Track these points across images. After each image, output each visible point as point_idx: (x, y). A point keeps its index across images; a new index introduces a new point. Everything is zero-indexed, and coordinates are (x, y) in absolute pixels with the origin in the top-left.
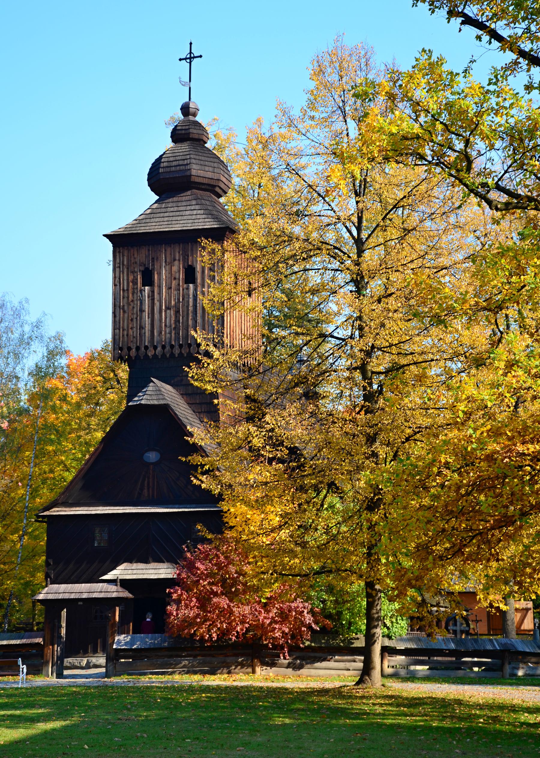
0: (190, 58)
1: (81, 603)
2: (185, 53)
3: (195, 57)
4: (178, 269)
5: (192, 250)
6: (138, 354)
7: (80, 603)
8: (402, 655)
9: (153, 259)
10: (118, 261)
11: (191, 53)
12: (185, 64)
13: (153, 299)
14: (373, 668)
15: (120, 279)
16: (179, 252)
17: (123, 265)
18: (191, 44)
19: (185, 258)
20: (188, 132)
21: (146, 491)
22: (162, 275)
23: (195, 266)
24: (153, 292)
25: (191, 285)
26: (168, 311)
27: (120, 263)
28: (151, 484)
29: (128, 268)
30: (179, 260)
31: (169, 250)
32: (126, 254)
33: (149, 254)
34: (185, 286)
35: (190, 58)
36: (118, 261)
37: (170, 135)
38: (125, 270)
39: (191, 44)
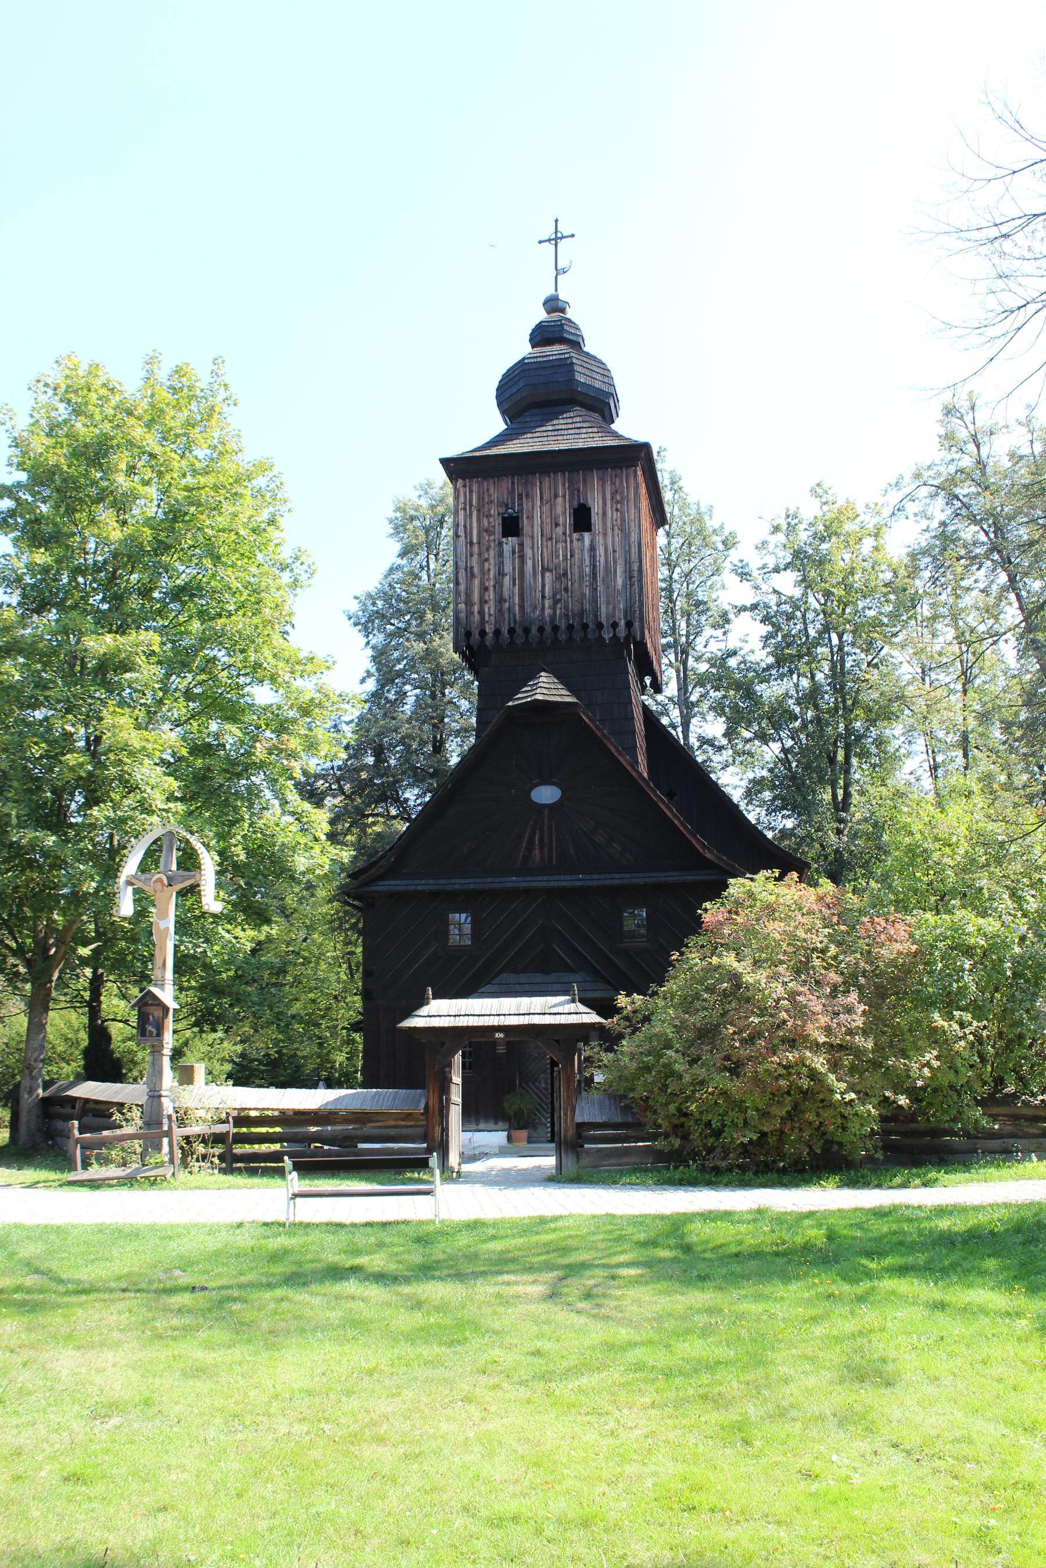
0: (556, 239)
1: (501, 1035)
2: (550, 233)
3: (563, 237)
4: (563, 509)
5: (585, 481)
7: (499, 1035)
9: (520, 496)
10: (462, 499)
11: (549, 240)
13: (522, 557)
14: (852, 1183)
17: (471, 505)
18: (556, 221)
19: (574, 491)
21: (537, 852)
24: (521, 545)
26: (548, 574)
28: (546, 841)
29: (479, 511)
30: (564, 497)
31: (546, 481)
32: (475, 488)
33: (513, 489)
34: (575, 536)
35: (556, 239)
36: (462, 499)
37: (496, 384)
39: (556, 221)
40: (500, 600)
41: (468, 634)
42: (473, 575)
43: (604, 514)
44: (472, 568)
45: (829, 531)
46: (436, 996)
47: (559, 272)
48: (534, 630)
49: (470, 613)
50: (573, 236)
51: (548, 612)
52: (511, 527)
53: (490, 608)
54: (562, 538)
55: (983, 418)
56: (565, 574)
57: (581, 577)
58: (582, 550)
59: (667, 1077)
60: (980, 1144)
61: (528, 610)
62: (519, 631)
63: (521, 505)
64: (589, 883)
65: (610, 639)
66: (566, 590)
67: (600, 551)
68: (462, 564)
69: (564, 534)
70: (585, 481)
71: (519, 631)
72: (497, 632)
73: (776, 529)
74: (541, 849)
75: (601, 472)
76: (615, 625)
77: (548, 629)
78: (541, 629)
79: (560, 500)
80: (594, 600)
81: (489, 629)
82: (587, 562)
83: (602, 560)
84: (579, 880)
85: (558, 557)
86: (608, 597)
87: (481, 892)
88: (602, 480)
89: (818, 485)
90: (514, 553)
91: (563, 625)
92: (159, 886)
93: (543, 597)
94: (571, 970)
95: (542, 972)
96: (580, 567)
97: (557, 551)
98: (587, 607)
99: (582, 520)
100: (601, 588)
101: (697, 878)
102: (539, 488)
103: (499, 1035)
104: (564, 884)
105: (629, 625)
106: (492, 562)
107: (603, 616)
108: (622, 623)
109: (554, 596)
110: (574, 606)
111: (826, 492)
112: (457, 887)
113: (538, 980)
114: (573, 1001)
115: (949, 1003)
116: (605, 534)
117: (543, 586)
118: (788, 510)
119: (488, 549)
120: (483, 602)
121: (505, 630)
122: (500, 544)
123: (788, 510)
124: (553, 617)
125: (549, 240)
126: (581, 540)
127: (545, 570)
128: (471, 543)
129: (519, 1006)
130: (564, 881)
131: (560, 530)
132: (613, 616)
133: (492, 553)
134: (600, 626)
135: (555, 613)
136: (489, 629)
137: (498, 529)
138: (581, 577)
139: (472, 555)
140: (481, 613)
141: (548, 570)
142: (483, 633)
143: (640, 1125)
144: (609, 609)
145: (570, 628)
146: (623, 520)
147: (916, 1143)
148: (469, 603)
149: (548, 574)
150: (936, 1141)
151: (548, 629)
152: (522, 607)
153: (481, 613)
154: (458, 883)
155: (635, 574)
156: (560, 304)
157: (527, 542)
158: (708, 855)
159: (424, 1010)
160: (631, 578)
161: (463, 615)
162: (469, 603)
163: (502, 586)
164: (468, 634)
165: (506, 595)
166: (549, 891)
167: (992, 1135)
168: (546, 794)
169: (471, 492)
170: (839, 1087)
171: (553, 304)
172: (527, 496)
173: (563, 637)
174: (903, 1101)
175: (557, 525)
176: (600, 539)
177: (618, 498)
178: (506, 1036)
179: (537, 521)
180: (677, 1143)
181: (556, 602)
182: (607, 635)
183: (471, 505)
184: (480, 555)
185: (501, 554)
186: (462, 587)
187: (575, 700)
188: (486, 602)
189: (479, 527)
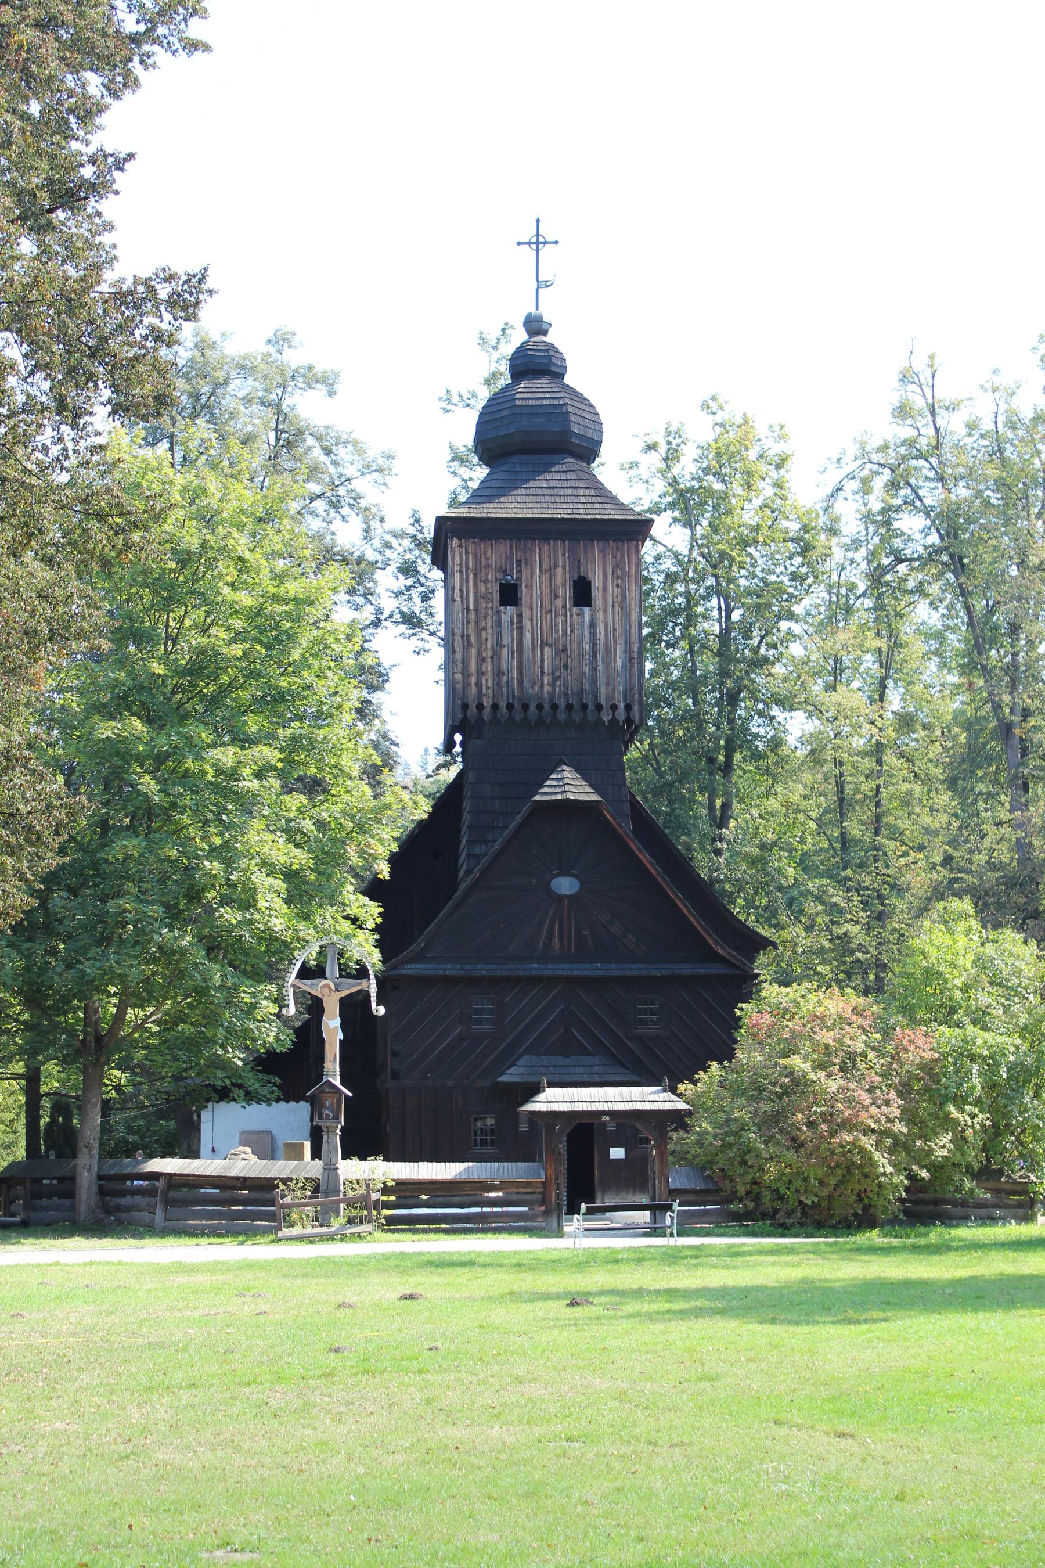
0: (538, 243)
2: (529, 234)
4: (563, 578)
5: (585, 552)
6: (525, 716)
7: (605, 1118)
8: (28, 1150)
9: (519, 562)
11: (529, 243)
12: (529, 252)
13: (520, 628)
15: (461, 590)
16: (564, 555)
17: (467, 568)
18: (538, 221)
19: (576, 564)
20: (536, 363)
22: (535, 589)
23: (590, 577)
24: (520, 616)
25: (586, 610)
26: (547, 649)
27: (461, 565)
29: (475, 575)
31: (546, 548)
34: (575, 610)
35: (538, 243)
38: (471, 577)
39: (538, 221)
40: (498, 673)
41: (465, 707)
42: (469, 644)
43: (605, 589)
44: (469, 636)
45: (723, 458)
46: (551, 1085)
47: (541, 285)
48: (533, 708)
49: (466, 685)
50: (556, 243)
51: (547, 689)
52: (509, 595)
53: (488, 681)
54: (561, 611)
55: (944, 392)
56: (565, 650)
57: (581, 655)
58: (582, 627)
59: (745, 1154)
60: (971, 1211)
61: (526, 685)
62: (518, 707)
63: (519, 572)
64: (609, 973)
65: (610, 721)
66: (566, 666)
67: (601, 628)
68: (458, 631)
69: (564, 607)
70: (585, 552)
71: (518, 707)
72: (495, 707)
73: (651, 447)
74: (561, 938)
75: (601, 544)
76: (614, 707)
77: (547, 706)
78: (540, 707)
79: (560, 570)
80: (594, 680)
81: (487, 703)
82: (587, 639)
83: (602, 638)
84: (596, 969)
85: (557, 631)
86: (608, 677)
87: (507, 980)
88: (602, 551)
89: (713, 398)
90: (512, 624)
91: (562, 703)
92: (326, 990)
93: (543, 672)
94: (586, 1052)
95: (563, 1055)
96: (580, 643)
97: (557, 625)
98: (587, 686)
99: (582, 594)
100: (600, 668)
101: (710, 971)
102: (540, 554)
103: (605, 1118)
104: (586, 973)
105: (628, 707)
106: (490, 631)
107: (603, 696)
108: (622, 705)
109: (553, 673)
110: (573, 685)
111: (721, 408)
112: (484, 973)
113: (560, 1063)
114: (665, 1091)
115: (960, 1101)
116: (605, 611)
117: (543, 660)
118: (669, 424)
119: (485, 617)
120: (480, 673)
121: (503, 705)
122: (498, 612)
123: (669, 424)
124: (552, 695)
125: (529, 243)
126: (581, 615)
127: (544, 644)
128: (468, 609)
129: (621, 1095)
130: (577, 970)
131: (559, 602)
132: (613, 698)
133: (489, 621)
134: (599, 707)
135: (554, 690)
136: (487, 703)
137: (497, 596)
138: (581, 655)
139: (468, 622)
140: (478, 684)
141: (547, 644)
142: (480, 707)
143: (718, 1191)
144: (610, 691)
145: (569, 707)
146: (624, 597)
147: (926, 1207)
148: (465, 673)
149: (547, 649)
150: (938, 1208)
151: (547, 706)
152: (520, 682)
153: (478, 684)
154: (483, 970)
155: (635, 655)
156: (544, 326)
157: (526, 613)
158: (720, 951)
159: (542, 1097)
160: (631, 659)
161: (459, 686)
162: (465, 673)
163: (500, 658)
164: (465, 707)
165: (504, 667)
166: (570, 980)
167: (981, 1205)
168: (565, 885)
169: (467, 553)
170: (883, 1163)
171: (535, 326)
172: (526, 563)
173: (562, 716)
174: (924, 1174)
175: (557, 597)
176: (600, 616)
177: (619, 572)
178: (612, 1119)
179: (536, 591)
180: (751, 1205)
181: (555, 679)
182: (606, 717)
183: (467, 568)
184: (477, 623)
185: (499, 623)
186: (458, 656)
187: (595, 797)
188: (483, 674)
189: (476, 593)
